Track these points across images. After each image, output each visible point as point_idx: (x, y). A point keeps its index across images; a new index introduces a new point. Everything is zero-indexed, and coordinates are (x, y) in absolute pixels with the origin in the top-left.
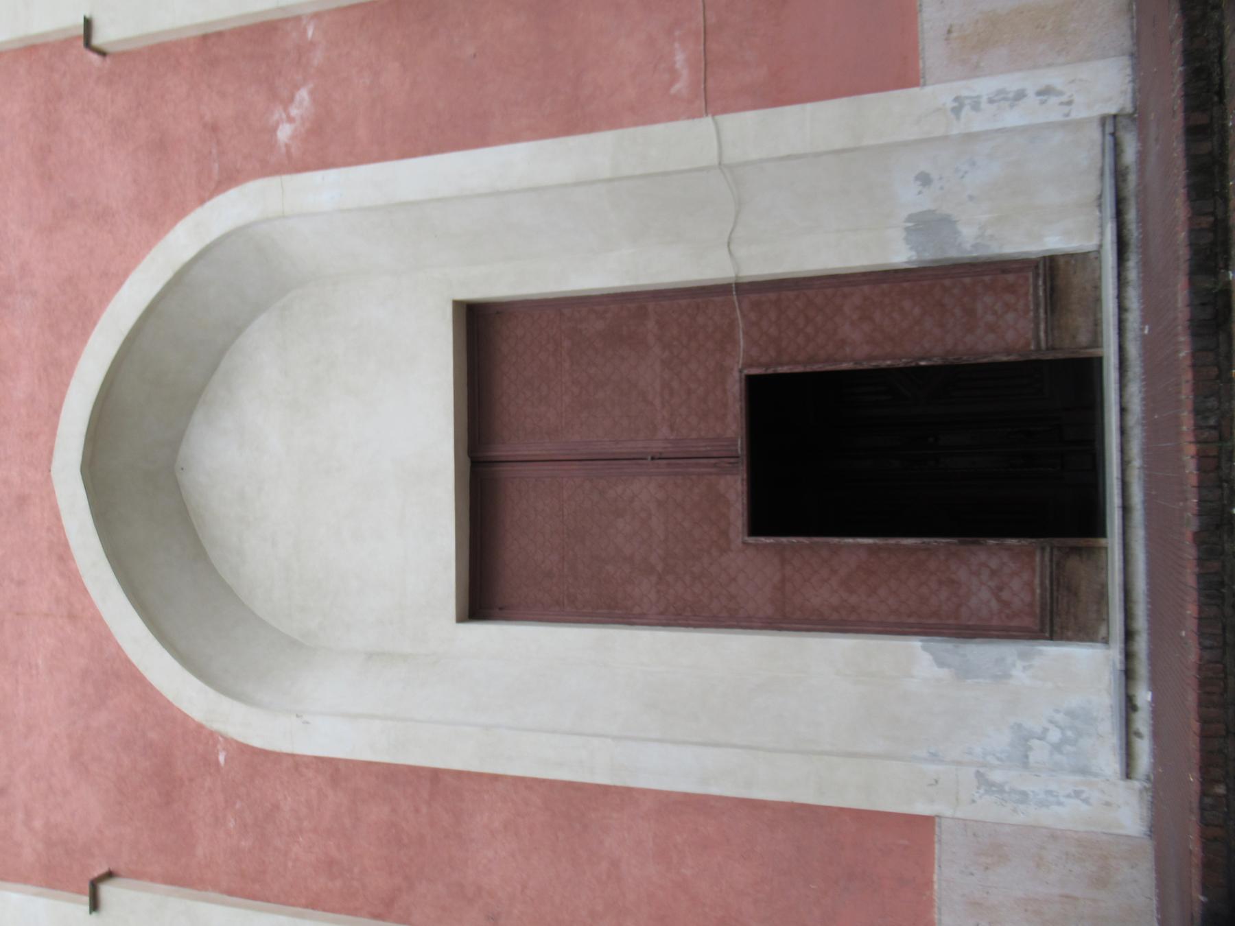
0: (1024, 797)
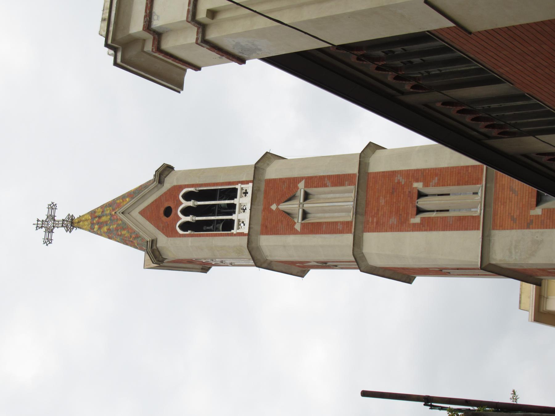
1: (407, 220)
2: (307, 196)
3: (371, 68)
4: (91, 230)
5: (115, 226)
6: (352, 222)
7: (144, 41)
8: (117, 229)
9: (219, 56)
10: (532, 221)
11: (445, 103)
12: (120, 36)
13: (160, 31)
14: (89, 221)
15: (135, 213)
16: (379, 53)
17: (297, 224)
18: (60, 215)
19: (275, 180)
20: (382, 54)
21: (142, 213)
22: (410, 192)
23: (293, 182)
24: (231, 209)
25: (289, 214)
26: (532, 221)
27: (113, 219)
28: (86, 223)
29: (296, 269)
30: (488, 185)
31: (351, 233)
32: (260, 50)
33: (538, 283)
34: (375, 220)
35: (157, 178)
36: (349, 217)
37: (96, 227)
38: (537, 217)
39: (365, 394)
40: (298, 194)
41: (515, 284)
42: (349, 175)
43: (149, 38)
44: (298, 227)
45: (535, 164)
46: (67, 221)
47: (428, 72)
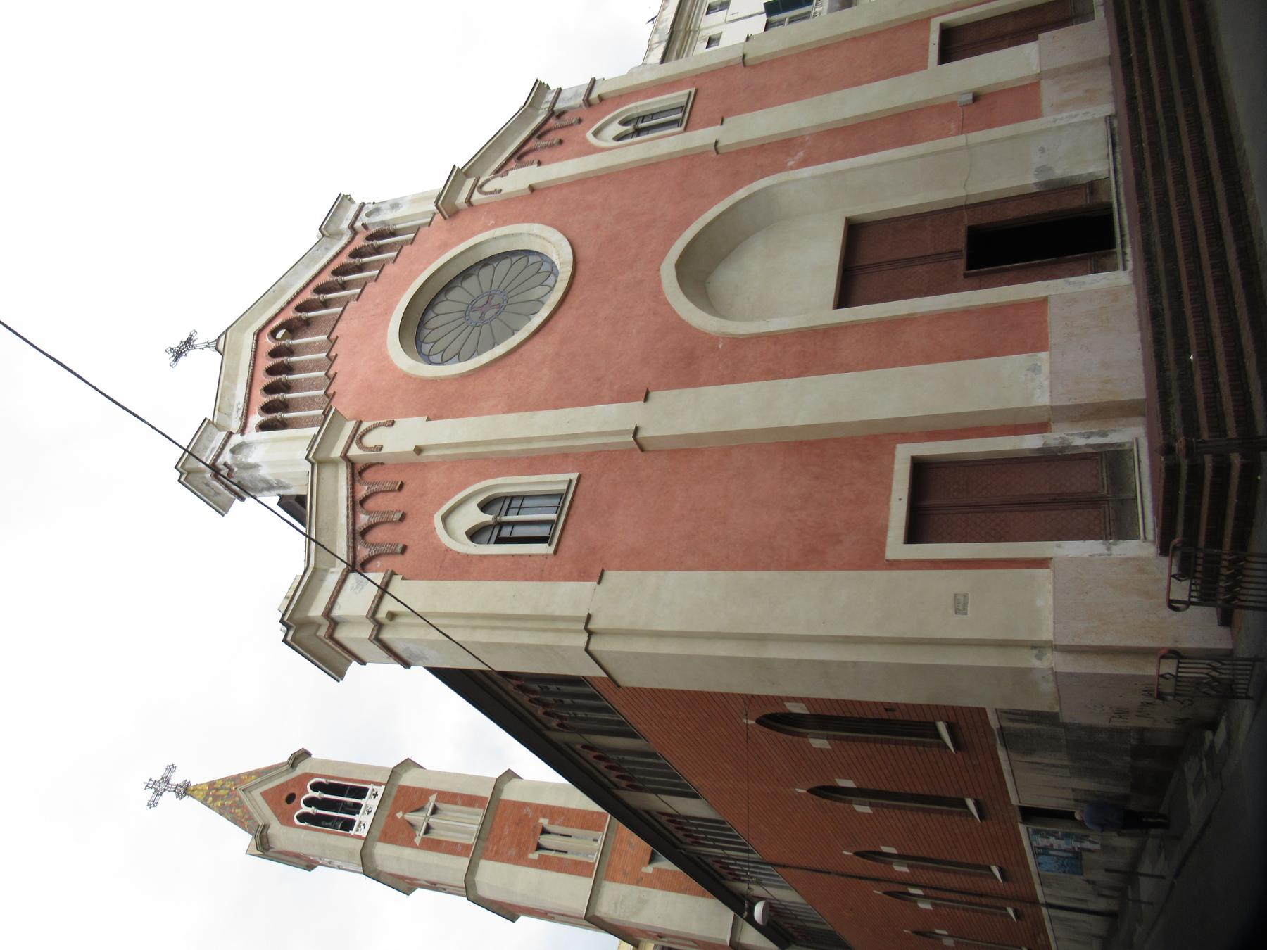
0: (1084, 283)
1: (525, 854)
2: (435, 811)
4: (204, 802)
5: (230, 802)
7: (319, 626)
8: (231, 806)
9: (387, 656)
11: (585, 747)
12: (298, 616)
13: (338, 621)
14: (205, 792)
15: (257, 793)
16: (535, 687)
18: (176, 779)
19: (408, 788)
20: (538, 688)
21: (264, 794)
23: (425, 793)
24: (356, 808)
25: (412, 825)
27: (231, 794)
28: (201, 793)
31: (468, 857)
32: (427, 659)
34: (495, 848)
35: (291, 763)
36: (471, 840)
37: (211, 799)
38: (647, 874)
40: (427, 806)
42: (481, 797)
43: (326, 623)
44: (417, 840)
46: (181, 787)
47: (575, 714)
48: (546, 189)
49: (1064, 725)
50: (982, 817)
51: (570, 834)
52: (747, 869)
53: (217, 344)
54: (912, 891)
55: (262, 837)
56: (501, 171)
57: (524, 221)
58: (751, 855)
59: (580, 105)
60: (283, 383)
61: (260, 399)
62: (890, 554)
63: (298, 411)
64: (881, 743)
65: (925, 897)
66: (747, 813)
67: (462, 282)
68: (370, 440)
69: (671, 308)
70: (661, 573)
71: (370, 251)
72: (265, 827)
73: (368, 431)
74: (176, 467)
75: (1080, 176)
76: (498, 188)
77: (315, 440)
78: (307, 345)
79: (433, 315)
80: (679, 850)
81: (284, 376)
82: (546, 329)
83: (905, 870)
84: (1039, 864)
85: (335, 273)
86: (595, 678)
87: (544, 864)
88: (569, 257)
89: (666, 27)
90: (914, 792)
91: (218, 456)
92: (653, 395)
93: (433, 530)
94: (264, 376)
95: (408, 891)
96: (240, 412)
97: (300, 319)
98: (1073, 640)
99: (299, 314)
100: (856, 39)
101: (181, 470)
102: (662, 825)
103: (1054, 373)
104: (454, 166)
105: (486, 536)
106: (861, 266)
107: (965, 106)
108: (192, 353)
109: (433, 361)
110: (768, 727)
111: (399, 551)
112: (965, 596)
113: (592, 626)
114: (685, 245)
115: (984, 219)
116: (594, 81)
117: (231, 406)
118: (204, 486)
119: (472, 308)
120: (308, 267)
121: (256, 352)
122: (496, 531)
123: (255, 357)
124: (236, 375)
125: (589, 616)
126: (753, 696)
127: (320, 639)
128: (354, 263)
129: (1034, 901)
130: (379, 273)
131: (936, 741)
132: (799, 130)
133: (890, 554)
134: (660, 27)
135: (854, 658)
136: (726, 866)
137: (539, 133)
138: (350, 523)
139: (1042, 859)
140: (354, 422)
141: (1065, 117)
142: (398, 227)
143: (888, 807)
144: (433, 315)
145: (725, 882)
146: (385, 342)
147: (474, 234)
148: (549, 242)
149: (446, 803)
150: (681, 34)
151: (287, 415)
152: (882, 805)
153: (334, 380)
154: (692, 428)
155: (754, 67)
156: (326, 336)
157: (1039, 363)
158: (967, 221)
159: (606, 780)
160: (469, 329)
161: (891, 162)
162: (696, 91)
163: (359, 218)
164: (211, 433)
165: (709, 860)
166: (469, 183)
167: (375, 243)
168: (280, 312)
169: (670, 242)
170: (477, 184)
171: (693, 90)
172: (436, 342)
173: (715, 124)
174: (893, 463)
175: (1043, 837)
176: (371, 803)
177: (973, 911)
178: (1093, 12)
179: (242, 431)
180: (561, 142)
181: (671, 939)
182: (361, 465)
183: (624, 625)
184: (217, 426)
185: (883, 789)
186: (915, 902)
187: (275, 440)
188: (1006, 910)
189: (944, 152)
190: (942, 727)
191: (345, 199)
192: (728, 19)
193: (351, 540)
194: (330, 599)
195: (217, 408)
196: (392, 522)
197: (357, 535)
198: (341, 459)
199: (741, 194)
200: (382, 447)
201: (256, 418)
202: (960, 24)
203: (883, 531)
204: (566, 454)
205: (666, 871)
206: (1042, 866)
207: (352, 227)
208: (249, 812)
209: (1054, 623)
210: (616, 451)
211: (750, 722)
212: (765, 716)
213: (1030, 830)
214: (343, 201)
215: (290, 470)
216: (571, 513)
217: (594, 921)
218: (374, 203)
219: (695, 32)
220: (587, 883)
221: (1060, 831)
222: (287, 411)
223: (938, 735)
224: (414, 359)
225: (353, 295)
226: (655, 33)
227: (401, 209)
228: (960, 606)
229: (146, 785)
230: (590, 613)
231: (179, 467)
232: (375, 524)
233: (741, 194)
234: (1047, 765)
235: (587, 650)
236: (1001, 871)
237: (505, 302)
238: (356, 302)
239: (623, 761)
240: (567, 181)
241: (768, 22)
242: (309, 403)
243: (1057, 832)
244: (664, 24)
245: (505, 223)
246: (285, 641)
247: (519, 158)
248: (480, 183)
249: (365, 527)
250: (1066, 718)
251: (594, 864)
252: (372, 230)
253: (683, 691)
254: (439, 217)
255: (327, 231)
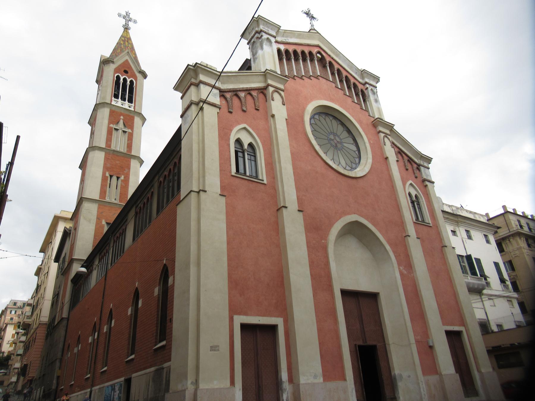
0: (352, 396)
1: (108, 171)
2: (124, 132)
3: (171, 167)
4: (122, 36)
5: (123, 47)
6: (111, 148)
7: (196, 79)
8: (121, 47)
9: (185, 108)
10: (99, 220)
11: (152, 192)
12: (199, 70)
13: (199, 87)
14: (126, 36)
15: (127, 58)
16: (176, 171)
17: (113, 125)
18: (131, 24)
19: (134, 120)
20: (175, 172)
21: (127, 61)
22: (120, 174)
23: (132, 128)
24: (123, 99)
25: (118, 123)
26: (99, 220)
27: (126, 47)
28: (126, 35)
29: (92, 120)
30: (118, 205)
31: (106, 147)
32: (185, 125)
33: (71, 219)
34: (110, 158)
35: (141, 71)
36: (113, 147)
37: (123, 39)
38: (101, 222)
39: (18, 138)
40: (126, 128)
41: (72, 209)
42: (131, 151)
43: (197, 82)
44: (111, 125)
45: (122, 223)
46: (128, 26)
47: (165, 188)
48: (387, 164)
49: (164, 395)
50: (127, 362)
51: (110, 187)
52: (100, 264)
53: (313, 30)
54: (96, 334)
55: (108, 61)
56: (393, 145)
57: (373, 156)
58: (110, 265)
59: (423, 177)
60: (298, 58)
61: (291, 49)
62: (236, 317)
63: (295, 64)
64: (157, 317)
65: (94, 339)
66: (127, 262)
67: (346, 130)
68: (276, 95)
69: (338, 220)
70: (225, 221)
71: (357, 91)
72: (113, 62)
73: (280, 94)
74: (259, 15)
75: (399, 394)
76: (386, 144)
77: (275, 73)
78: (315, 67)
79: (331, 119)
80: (111, 234)
81: (301, 58)
82: (327, 167)
83: (105, 330)
84: (108, 387)
85: (346, 77)
86: (180, 196)
87: (104, 179)
88: (358, 176)
89: (459, 212)
90: (137, 333)
91: (265, 33)
92: (301, 213)
93: (239, 124)
94: (301, 50)
95: (89, 123)
96: (285, 41)
97: (326, 63)
98: (199, 397)
99: (328, 63)
100: (455, 295)
101: (258, 18)
102: (121, 227)
103: (314, 384)
104: (394, 125)
105: (238, 146)
106: (359, 300)
107: (428, 342)
108: (308, 19)
109: (312, 120)
110: (162, 269)
111: (230, 110)
112: (218, 350)
113: (201, 193)
114: (365, 224)
115: (380, 353)
116: (433, 183)
117: (287, 37)
118: (252, 28)
119: (335, 135)
120: (348, 66)
121: (311, 46)
122: (240, 150)
123: (308, 45)
124: (300, 38)
125: (205, 191)
126: (175, 262)
127: (191, 79)
128: (351, 85)
129: (93, 386)
130: (348, 96)
131: (158, 341)
132: (415, 271)
133: (236, 317)
134: (459, 210)
135: (191, 304)
136: (105, 255)
137: (410, 160)
138: (240, 89)
139: (110, 388)
140: (283, 88)
141: (423, 386)
142: (368, 102)
143: (131, 322)
144: (331, 119)
145: (98, 255)
146: (318, 99)
147: (366, 134)
148: (364, 167)
149: (128, 136)
150: (456, 219)
151: (285, 60)
152: (131, 319)
153: (301, 79)
154: (287, 231)
155: (442, 251)
156: (319, 75)
157: (318, 378)
158: (379, 345)
159: (139, 202)
160: (326, 135)
161: (403, 312)
162: (431, 227)
163: (370, 86)
164: (275, 29)
165: (107, 248)
166: (388, 132)
167: (360, 93)
168: (328, 55)
169: (367, 219)
170: (387, 135)
171: (431, 225)
172: (320, 121)
173: (417, 235)
174: (275, 317)
175: (119, 388)
176: (126, 105)
177: (89, 360)
178: (468, 397)
179: (277, 42)
180: (407, 170)
181: (74, 234)
182: (265, 92)
183: (202, 206)
184: (278, 31)
185: (138, 320)
186: (92, 335)
187: (273, 56)
188: (89, 374)
189: (408, 334)
190: (164, 343)
191: (378, 80)
192: (463, 239)
193: (233, 90)
194: (207, 83)
195: (286, 31)
196: (242, 107)
197: (235, 92)
198: (267, 84)
199: (388, 247)
200: (274, 101)
201: (282, 47)
202: (462, 340)
203: (246, 314)
204: (275, 178)
205: (103, 230)
206: (107, 388)
207: (366, 83)
208: (119, 55)
209: (207, 389)
210: (277, 199)
211: (165, 261)
212: (167, 268)
213: (122, 383)
214: (377, 79)
215: (261, 63)
216: (250, 182)
217: (81, 201)
218: (377, 92)
219: (458, 225)
220: (97, 197)
221: (122, 395)
222: (294, 60)
223: (160, 341)
224: (311, 112)
225: (337, 85)
226: (456, 208)
227: (375, 103)
228: (214, 348)
229: (127, 12)
230: (207, 192)
231: (259, 17)
232: (241, 100)
233: (388, 247)
234: (148, 389)
235: (191, 191)
236: (105, 371)
237: (338, 149)
238: (335, 86)
239: (147, 209)
240: (390, 173)
241: (462, 256)
242: (290, 69)
243: (121, 394)
244: (460, 212)
245: (371, 148)
246: (188, 65)
247: (399, 152)
248: (388, 136)
249: (239, 95)
250: (167, 395)
251: (105, 199)
252: (366, 92)
253: (176, 233)
254: (372, 119)
255: (364, 73)
